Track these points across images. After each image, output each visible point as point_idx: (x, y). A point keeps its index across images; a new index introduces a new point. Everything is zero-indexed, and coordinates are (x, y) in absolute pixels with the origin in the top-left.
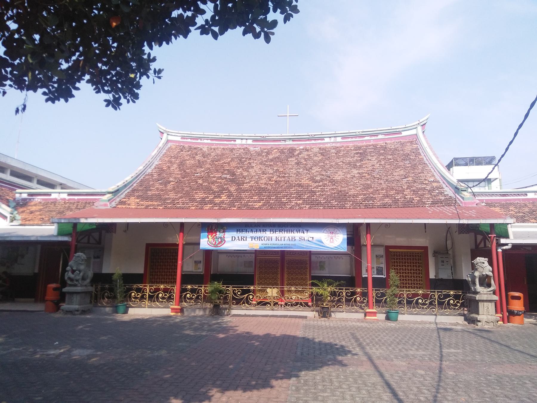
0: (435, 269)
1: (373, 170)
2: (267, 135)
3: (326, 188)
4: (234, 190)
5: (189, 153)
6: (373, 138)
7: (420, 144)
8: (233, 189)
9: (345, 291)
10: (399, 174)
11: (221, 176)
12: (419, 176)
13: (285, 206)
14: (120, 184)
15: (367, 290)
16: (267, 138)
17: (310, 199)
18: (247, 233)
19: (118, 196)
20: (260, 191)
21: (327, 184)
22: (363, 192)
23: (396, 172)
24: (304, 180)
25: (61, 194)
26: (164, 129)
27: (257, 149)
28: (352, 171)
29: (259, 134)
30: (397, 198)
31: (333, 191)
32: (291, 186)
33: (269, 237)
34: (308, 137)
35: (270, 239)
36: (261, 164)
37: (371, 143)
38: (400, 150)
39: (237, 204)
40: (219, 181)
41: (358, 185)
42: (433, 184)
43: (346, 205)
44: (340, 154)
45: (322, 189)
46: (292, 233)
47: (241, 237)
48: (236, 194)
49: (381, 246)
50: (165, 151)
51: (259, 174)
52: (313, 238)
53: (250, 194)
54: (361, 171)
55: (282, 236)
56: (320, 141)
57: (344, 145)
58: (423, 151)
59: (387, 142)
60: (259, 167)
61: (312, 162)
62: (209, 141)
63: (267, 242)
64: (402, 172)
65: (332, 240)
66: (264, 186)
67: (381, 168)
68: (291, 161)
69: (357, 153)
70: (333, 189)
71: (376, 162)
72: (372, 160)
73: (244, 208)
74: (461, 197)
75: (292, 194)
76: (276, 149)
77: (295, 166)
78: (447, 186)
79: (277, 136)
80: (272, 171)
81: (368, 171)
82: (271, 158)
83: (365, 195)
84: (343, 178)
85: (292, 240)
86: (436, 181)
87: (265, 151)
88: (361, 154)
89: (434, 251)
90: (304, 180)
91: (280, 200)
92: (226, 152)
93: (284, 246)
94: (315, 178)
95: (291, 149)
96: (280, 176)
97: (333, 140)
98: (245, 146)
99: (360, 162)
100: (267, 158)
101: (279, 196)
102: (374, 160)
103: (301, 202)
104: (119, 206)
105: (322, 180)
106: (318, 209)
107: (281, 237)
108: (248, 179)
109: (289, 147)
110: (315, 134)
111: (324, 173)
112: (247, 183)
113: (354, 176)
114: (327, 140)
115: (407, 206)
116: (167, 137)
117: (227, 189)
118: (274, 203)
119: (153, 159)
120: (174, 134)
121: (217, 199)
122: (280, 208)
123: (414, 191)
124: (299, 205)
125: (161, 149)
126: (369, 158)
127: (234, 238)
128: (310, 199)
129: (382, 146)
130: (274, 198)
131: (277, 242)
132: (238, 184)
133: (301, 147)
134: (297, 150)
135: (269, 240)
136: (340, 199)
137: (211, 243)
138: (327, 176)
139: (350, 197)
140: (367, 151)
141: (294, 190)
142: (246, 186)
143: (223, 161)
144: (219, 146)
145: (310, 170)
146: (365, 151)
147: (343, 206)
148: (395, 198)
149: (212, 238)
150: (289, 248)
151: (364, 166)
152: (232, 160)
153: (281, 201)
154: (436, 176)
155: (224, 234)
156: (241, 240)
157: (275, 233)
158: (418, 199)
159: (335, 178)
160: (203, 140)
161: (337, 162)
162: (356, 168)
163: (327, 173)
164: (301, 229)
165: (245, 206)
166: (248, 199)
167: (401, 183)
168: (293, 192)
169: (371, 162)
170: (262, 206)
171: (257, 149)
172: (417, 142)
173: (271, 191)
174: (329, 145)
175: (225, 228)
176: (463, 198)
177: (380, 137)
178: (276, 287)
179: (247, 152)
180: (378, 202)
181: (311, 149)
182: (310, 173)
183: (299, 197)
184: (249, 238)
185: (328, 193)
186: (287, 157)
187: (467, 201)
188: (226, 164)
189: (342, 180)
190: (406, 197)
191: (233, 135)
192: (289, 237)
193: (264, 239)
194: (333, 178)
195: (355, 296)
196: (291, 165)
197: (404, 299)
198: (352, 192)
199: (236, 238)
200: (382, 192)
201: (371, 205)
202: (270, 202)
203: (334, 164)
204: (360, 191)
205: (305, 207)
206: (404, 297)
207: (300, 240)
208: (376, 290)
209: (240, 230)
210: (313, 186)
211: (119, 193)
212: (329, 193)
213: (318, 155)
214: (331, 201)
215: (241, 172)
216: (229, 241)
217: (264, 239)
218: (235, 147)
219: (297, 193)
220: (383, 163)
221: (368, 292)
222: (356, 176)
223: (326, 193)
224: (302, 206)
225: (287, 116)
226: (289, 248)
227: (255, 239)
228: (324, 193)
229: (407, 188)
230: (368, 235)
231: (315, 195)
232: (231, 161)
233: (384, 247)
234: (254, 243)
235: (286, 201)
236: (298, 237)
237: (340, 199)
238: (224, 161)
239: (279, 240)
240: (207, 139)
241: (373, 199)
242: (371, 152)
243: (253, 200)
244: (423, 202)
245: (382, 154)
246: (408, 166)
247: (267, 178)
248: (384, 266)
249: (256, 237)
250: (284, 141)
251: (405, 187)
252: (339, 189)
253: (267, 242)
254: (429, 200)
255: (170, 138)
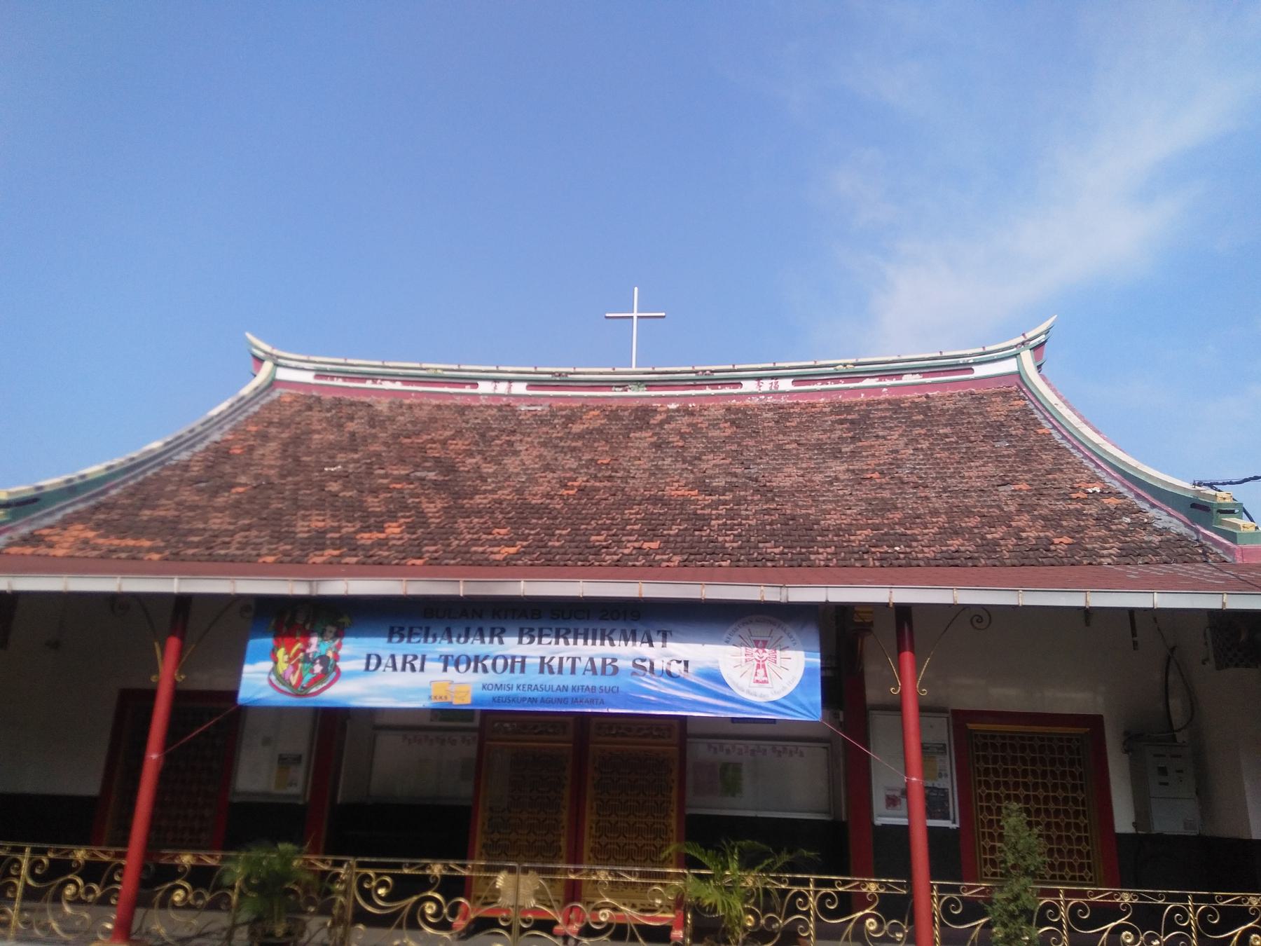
0: (1134, 792)
1: (897, 463)
2: (571, 370)
3: (742, 507)
4: (435, 510)
5: (329, 415)
6: (888, 382)
7: (1033, 399)
8: (433, 507)
9: (816, 892)
10: (981, 474)
11: (408, 475)
12: (1049, 480)
13: (598, 557)
14: (51, 481)
15: (910, 886)
16: (570, 377)
17: (688, 539)
18: (430, 639)
19: (33, 519)
20: (522, 514)
21: (749, 498)
22: (870, 522)
23: (970, 467)
24: (673, 488)
25: (514, 385)
26: (268, 348)
27: (539, 408)
28: (830, 464)
29: (547, 369)
30: (989, 536)
31: (766, 517)
32: (629, 502)
33: (513, 658)
34: (693, 375)
35: (518, 666)
36: (544, 444)
37: (882, 397)
38: (976, 414)
39: (433, 548)
40: (398, 486)
41: (851, 501)
42: (1105, 501)
43: (813, 557)
44: (788, 424)
45: (729, 512)
46: (607, 642)
47: (405, 657)
48: (438, 521)
49: (943, 710)
50: (256, 408)
51: (533, 469)
52: (686, 663)
53: (485, 523)
54: (857, 466)
55: (565, 655)
56: (727, 390)
57: (800, 401)
58: (1048, 415)
59: (930, 394)
60: (535, 453)
61: (703, 443)
62: (398, 386)
63: (506, 678)
64: (991, 469)
65: (761, 671)
66: (539, 501)
67: (921, 457)
68: (641, 439)
69: (841, 422)
70: (767, 512)
71: (902, 443)
72: (889, 437)
73: (452, 562)
74: (1218, 532)
75: (628, 522)
76: (598, 408)
77: (651, 453)
78: (1153, 506)
79: (601, 373)
80: (577, 464)
81: (879, 465)
82: (578, 431)
83: (875, 528)
84: (802, 483)
85: (604, 672)
86: (1107, 493)
87: (564, 413)
88: (852, 422)
89: (1126, 733)
90: (673, 488)
91: (584, 538)
92: (443, 414)
93: (570, 694)
94: (711, 483)
95: (640, 409)
96: (599, 475)
97: (766, 385)
98: (505, 399)
99: (851, 443)
100: (567, 430)
101: (583, 527)
102: (896, 438)
103: (654, 545)
104: (14, 550)
105: (731, 487)
106: (712, 566)
107: (561, 659)
108: (493, 482)
109: (636, 403)
110: (713, 368)
111: (738, 471)
112: (485, 492)
113: (837, 479)
114: (749, 386)
115: (1034, 562)
116: (273, 372)
117: (417, 507)
118: (562, 547)
119: (206, 426)
120: (294, 364)
121: (366, 535)
122: (580, 563)
123: (1044, 518)
124: (647, 554)
125: (244, 403)
126: (881, 434)
127: (374, 661)
128: (688, 539)
129: (915, 405)
130: (564, 532)
131: (546, 679)
132: (457, 496)
133: (673, 406)
134: (660, 413)
135: (512, 671)
136: (793, 538)
137: (282, 679)
138: (750, 479)
139: (826, 533)
140: (871, 416)
141: (637, 513)
142: (479, 501)
143: (425, 437)
144: (425, 400)
145: (696, 462)
146: (866, 416)
147: (802, 560)
148: (983, 538)
149: (290, 660)
150: (591, 702)
151: (864, 454)
152: (459, 433)
153: (589, 541)
154: (1107, 480)
155: (339, 647)
156: (404, 669)
157: (540, 643)
158: (1066, 540)
159: (774, 484)
160: (379, 381)
161: (781, 442)
162: (842, 458)
163: (746, 471)
164: (641, 629)
165: (455, 554)
166: (475, 536)
167: (996, 497)
168: (631, 517)
169: (885, 442)
170: (516, 557)
171: (539, 408)
172: (1022, 394)
173: (559, 513)
174: (756, 400)
175: (346, 620)
176: (1232, 537)
177: (908, 379)
178: (533, 869)
179: (507, 416)
180: (926, 550)
181: (700, 410)
182: (695, 470)
183: (649, 533)
184: (433, 660)
185: (750, 522)
186: (628, 430)
187: (1248, 546)
188: (434, 443)
189: (797, 490)
190: (1024, 535)
191: (469, 368)
192: (591, 660)
193: (494, 665)
194: (768, 484)
195: (859, 914)
196: (638, 448)
197: (1062, 929)
198: (832, 520)
199: (384, 661)
200: (934, 520)
201: (902, 556)
202: (550, 544)
203: (770, 447)
204: (859, 517)
205: (669, 560)
206: (1061, 921)
207: (634, 673)
208: (942, 889)
209: (402, 629)
210: (700, 502)
211: (39, 510)
212: (753, 522)
213: (722, 426)
214: (761, 545)
215: (476, 463)
216: (353, 674)
217: (494, 665)
218: (473, 404)
219: (648, 519)
220: (925, 445)
221: (909, 897)
222: (842, 477)
223: (744, 522)
224: (658, 557)
225: (632, 317)
226: (591, 702)
227: (457, 664)
228: (736, 522)
229: (1019, 512)
230: (907, 655)
231: (705, 528)
232: (453, 438)
233: (949, 715)
234: (452, 682)
235: (604, 544)
236: (628, 659)
237: (793, 538)
238: (429, 437)
239: (551, 672)
240: (393, 377)
241: (909, 540)
242: (885, 417)
243: (490, 537)
244: (1086, 550)
245: (916, 424)
246: (1005, 453)
247: (554, 481)
248: (948, 783)
249: (464, 658)
250: (621, 389)
251: (1012, 508)
252: (788, 512)
253: (506, 678)
254: (1107, 545)
255: (282, 374)
